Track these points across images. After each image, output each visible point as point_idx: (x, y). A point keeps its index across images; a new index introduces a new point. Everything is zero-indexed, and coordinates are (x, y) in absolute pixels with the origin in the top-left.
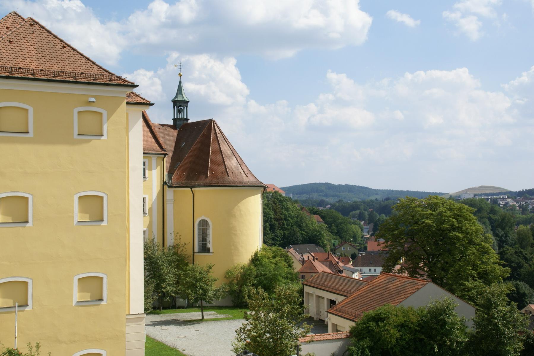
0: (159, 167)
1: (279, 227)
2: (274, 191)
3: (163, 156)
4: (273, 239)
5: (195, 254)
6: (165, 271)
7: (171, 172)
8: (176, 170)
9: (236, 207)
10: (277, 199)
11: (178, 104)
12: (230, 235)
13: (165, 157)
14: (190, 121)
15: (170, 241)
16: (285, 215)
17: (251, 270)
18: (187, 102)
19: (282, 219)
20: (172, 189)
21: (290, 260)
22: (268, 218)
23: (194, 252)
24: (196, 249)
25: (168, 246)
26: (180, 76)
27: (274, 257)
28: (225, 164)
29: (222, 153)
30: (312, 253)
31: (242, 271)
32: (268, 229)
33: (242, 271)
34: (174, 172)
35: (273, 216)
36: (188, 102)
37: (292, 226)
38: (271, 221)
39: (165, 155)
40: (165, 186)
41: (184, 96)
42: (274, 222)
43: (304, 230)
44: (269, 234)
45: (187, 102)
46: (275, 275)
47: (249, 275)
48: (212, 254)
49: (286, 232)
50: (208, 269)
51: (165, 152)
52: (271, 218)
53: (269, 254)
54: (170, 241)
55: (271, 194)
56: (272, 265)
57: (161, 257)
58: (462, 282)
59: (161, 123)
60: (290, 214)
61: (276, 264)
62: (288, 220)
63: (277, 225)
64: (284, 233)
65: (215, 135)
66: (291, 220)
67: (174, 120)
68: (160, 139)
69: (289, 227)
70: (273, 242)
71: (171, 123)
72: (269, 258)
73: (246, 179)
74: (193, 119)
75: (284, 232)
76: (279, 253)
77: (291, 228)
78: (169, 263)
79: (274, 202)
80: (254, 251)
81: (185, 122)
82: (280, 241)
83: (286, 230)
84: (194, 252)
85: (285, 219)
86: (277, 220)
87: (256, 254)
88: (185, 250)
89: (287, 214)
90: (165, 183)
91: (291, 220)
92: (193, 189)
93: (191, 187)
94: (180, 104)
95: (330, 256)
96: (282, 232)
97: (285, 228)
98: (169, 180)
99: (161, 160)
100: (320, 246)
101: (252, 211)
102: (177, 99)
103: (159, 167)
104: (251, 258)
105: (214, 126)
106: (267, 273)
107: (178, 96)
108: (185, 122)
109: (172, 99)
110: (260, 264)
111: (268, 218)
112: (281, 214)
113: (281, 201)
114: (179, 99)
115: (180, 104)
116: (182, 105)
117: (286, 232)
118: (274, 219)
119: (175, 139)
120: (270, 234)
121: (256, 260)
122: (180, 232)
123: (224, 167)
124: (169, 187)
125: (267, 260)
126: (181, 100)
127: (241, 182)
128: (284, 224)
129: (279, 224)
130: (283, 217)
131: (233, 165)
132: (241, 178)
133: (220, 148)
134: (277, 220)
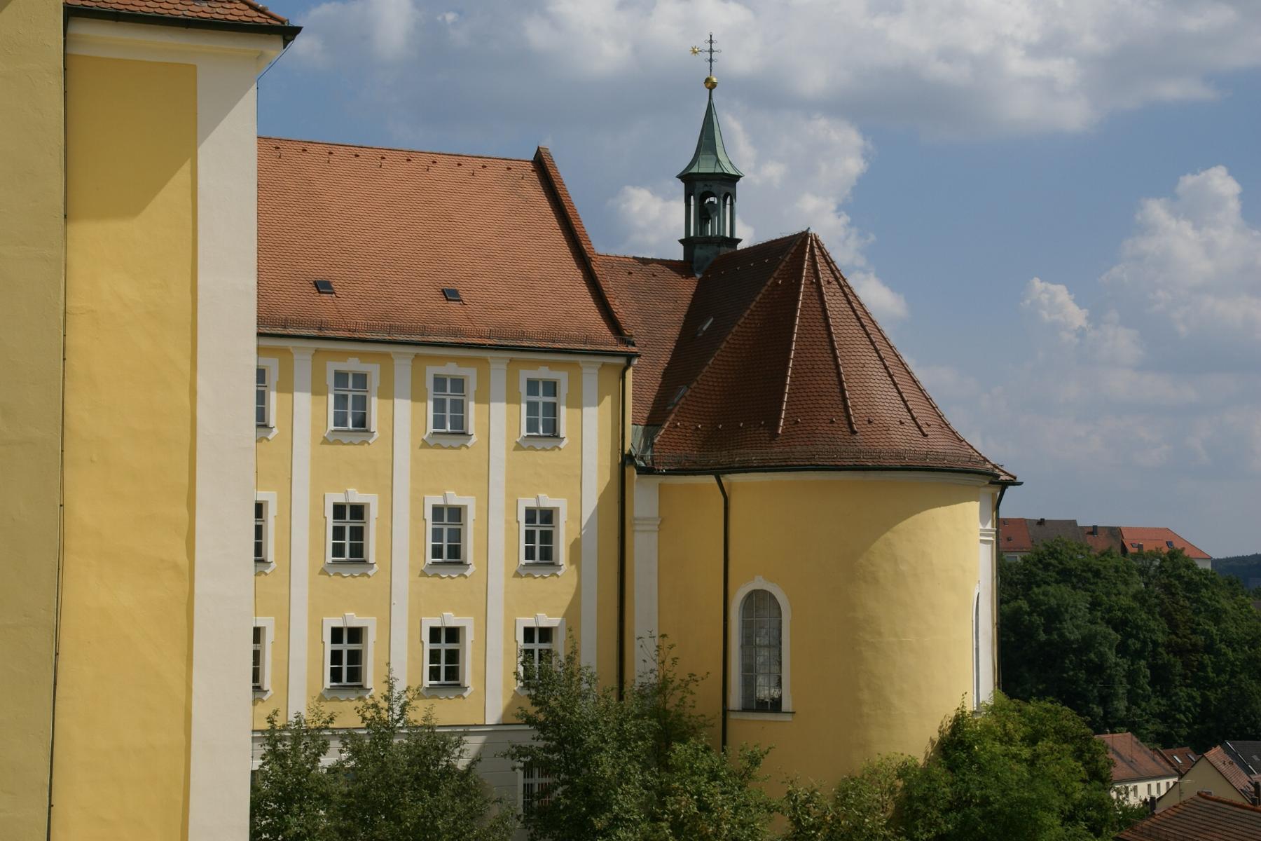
0: (608, 399)
1: (1185, 677)
2: (1166, 550)
3: (622, 361)
4: (1163, 717)
5: (732, 716)
6: (606, 766)
7: (652, 423)
8: (670, 412)
10: (1179, 577)
11: (700, 187)
12: (855, 651)
13: (629, 364)
14: (740, 247)
15: (642, 667)
16: (1206, 633)
17: (931, 780)
18: (735, 178)
19: (1195, 648)
20: (654, 481)
21: (1098, 752)
22: (1144, 643)
23: (725, 711)
24: (735, 700)
25: (638, 681)
26: (710, 85)
27: (1032, 740)
28: (843, 391)
29: (833, 350)
31: (900, 783)
32: (1143, 681)
33: (900, 783)
34: (664, 421)
35: (1161, 638)
36: (737, 178)
37: (1233, 674)
38: (1155, 654)
39: (630, 357)
40: (627, 470)
41: (721, 156)
42: (1165, 657)
44: (1147, 698)
45: (735, 178)
46: (1024, 802)
47: (924, 799)
48: (788, 718)
49: (1211, 695)
50: (746, 764)
51: (634, 349)
52: (1155, 643)
53: (1017, 728)
54: (642, 667)
55: (1157, 563)
56: (1017, 767)
57: (595, 722)
59: (641, 256)
60: (1225, 631)
61: (1032, 763)
62: (1218, 653)
63: (1179, 668)
64: (1206, 700)
65: (813, 289)
66: (1230, 654)
67: (687, 242)
68: (616, 305)
69: (1224, 677)
70: (1162, 728)
71: (678, 254)
72: (1007, 739)
73: (921, 445)
74: (747, 235)
75: (1203, 695)
76: (1050, 726)
77: (1228, 682)
78: (623, 742)
79: (1167, 588)
81: (725, 250)
82: (1189, 725)
83: (1213, 686)
84: (725, 711)
85: (1209, 648)
86: (1178, 651)
87: (959, 722)
88: (689, 700)
89: (1214, 630)
90: (626, 461)
91: (1230, 654)
92: (725, 479)
93: (718, 472)
94: (708, 188)
96: (1196, 694)
97: (1206, 678)
98: (646, 448)
99: (615, 376)
101: (951, 569)
102: (694, 170)
103: (608, 399)
105: (813, 256)
106: (993, 794)
107: (702, 157)
108: (725, 250)
109: (681, 167)
110: (973, 759)
111: (1144, 643)
112: (1194, 632)
113: (1191, 587)
114: (705, 167)
115: (708, 188)
116: (714, 189)
118: (1169, 647)
119: (685, 309)
120: (1153, 701)
121: (956, 743)
122: (676, 634)
123: (838, 399)
124: (643, 471)
125: (998, 748)
126: (711, 171)
127: (898, 455)
128: (1202, 667)
129: (1186, 665)
130: (1200, 640)
131: (873, 395)
132: (903, 439)
133: (830, 334)
134: (1178, 651)
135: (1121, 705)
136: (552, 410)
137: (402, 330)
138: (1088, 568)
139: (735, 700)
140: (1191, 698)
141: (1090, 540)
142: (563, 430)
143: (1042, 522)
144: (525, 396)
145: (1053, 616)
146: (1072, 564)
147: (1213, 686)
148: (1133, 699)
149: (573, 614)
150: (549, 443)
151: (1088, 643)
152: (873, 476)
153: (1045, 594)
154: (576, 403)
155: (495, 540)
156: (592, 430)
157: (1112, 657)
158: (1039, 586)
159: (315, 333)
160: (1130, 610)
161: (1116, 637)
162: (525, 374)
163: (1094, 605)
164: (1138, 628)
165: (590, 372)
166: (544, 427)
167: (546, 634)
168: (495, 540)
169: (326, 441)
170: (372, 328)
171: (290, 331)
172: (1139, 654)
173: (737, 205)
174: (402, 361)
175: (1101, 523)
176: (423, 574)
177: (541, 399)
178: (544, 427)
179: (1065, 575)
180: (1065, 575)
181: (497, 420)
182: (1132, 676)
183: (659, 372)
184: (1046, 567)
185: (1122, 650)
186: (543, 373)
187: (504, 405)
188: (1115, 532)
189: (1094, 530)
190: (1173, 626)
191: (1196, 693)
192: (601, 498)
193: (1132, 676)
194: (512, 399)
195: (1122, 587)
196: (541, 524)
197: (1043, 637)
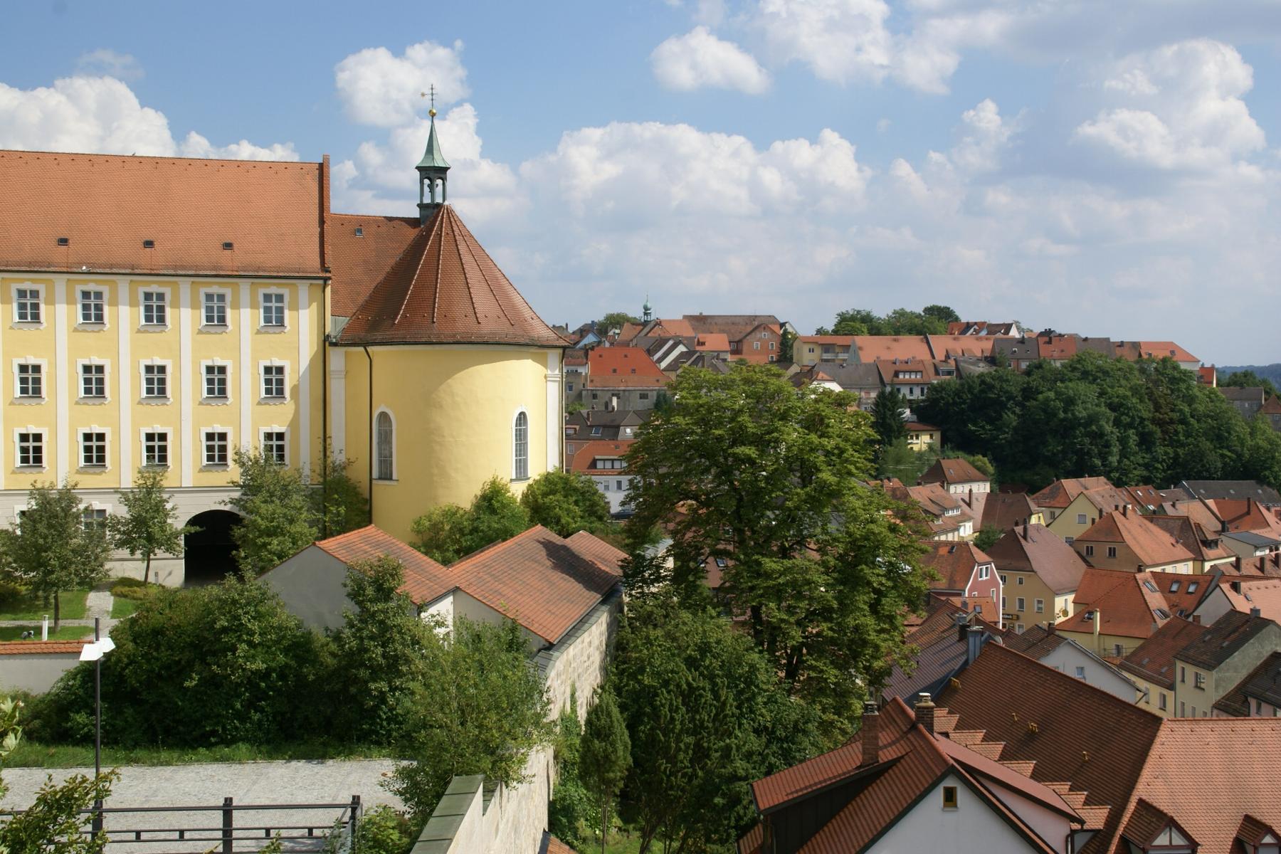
0: (314, 305)
3: (321, 282)
9: (443, 386)
16: (1181, 411)
19: (1172, 422)
24: (375, 474)
30: (1210, 502)
35: (1145, 414)
39: (326, 279)
43: (1228, 448)
49: (1180, 451)
51: (328, 275)
52: (1142, 420)
58: (756, 557)
63: (1159, 434)
64: (1177, 454)
66: (1196, 426)
67: (422, 206)
69: (1190, 440)
70: (1145, 473)
71: (415, 213)
80: (489, 478)
82: (1164, 471)
83: (1183, 445)
85: (1183, 421)
86: (1159, 423)
89: (1187, 409)
91: (1196, 426)
92: (369, 349)
93: (365, 345)
95: (1253, 508)
97: (1179, 441)
100: (1269, 485)
104: (479, 493)
111: (1133, 418)
112: (1172, 411)
117: (1180, 451)
118: (1154, 421)
128: (1176, 433)
130: (1175, 416)
132: (491, 324)
135: (1114, 460)
136: (280, 310)
137: (184, 267)
138: (1100, 369)
140: (1166, 453)
141: (1119, 351)
142: (286, 322)
143: (1086, 339)
144: (262, 304)
145: (1070, 402)
146: (1090, 368)
147: (1183, 445)
148: (1124, 454)
149: (294, 424)
150: (278, 330)
151: (1092, 419)
152: (437, 347)
153: (1066, 388)
154: (295, 307)
155: (246, 384)
156: (306, 321)
157: (1108, 428)
158: (1062, 381)
159: (128, 271)
160: (1125, 397)
161: (1112, 415)
162: (262, 291)
163: (1102, 394)
164: (1129, 409)
165: (303, 288)
166: (275, 319)
167: (280, 436)
168: (246, 384)
169: (139, 331)
170: (167, 267)
171: (114, 270)
172: (1130, 425)
173: (448, 184)
174: (185, 286)
175: (1125, 340)
176: (201, 404)
177: (274, 304)
178: (275, 319)
179: (1085, 375)
180: (1085, 375)
181: (245, 318)
182: (1123, 441)
183: (373, 286)
184: (1074, 369)
185: (1117, 423)
186: (273, 290)
187: (249, 310)
188: (1136, 346)
189: (1122, 344)
190: (1157, 408)
191: (1170, 450)
192: (311, 361)
193: (1123, 441)
194: (254, 306)
195: (1123, 382)
196: (274, 376)
197: (1062, 415)
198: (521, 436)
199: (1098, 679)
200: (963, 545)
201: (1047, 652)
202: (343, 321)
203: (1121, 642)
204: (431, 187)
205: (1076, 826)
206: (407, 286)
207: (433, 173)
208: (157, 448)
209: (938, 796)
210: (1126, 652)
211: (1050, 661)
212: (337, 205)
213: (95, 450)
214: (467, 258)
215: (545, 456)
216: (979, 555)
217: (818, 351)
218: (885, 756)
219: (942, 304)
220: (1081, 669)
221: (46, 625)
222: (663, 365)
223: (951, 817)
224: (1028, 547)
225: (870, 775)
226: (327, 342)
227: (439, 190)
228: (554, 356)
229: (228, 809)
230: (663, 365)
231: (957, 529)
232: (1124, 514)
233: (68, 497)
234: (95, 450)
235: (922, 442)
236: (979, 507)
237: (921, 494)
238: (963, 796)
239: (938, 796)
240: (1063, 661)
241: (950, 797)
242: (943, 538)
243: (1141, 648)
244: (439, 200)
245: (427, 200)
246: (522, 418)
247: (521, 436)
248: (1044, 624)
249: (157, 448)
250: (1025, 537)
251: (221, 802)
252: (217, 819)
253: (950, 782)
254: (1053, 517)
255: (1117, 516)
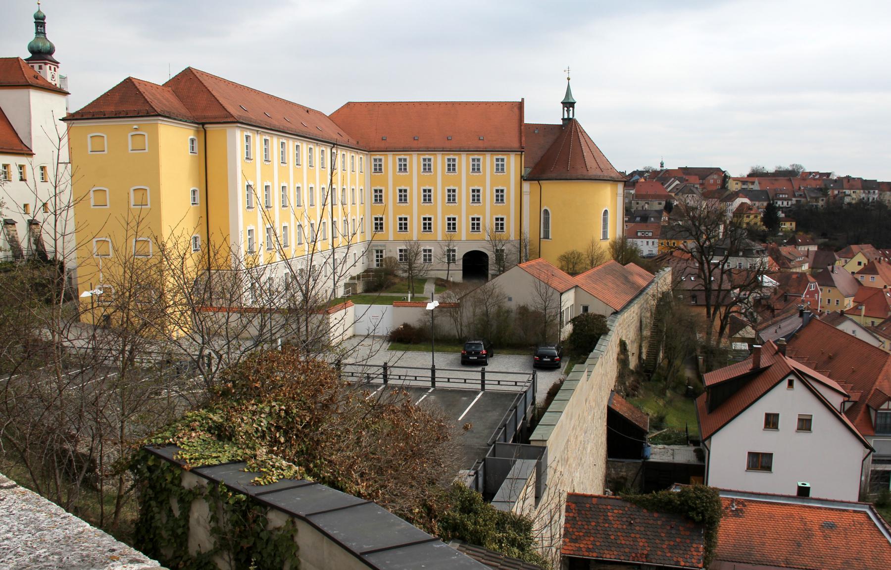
24: (542, 236)
93: (538, 180)
132: (594, 172)
139: (542, 236)
166: (500, 168)
198: (605, 220)
199: (862, 335)
200: (803, 275)
201: (840, 323)
202: (529, 170)
203: (873, 320)
204: (568, 111)
205: (846, 399)
206: (557, 153)
207: (568, 104)
208: (452, 225)
209: (785, 383)
210: (876, 324)
211: (841, 327)
212: (527, 120)
213: (427, 225)
214: (582, 140)
215: (616, 229)
216: (811, 279)
217: (740, 184)
218: (762, 366)
219: (786, 165)
220: (854, 332)
221: (410, 295)
222: (669, 189)
223: (790, 392)
224: (834, 276)
225: (757, 372)
226: (523, 179)
227: (571, 112)
228: (620, 188)
229: (385, 367)
230: (669, 189)
231: (801, 266)
232: (879, 262)
233: (418, 244)
234: (427, 225)
235: (788, 226)
236: (811, 257)
237: (785, 250)
238: (796, 383)
239: (785, 383)
240: (847, 327)
241: (791, 383)
242: (794, 270)
243: (883, 323)
244: (571, 116)
245: (566, 117)
246: (606, 212)
247: (605, 220)
248: (839, 311)
249: (452, 225)
250: (832, 271)
251: (382, 364)
252: (429, 374)
253: (791, 377)
254: (846, 262)
255: (876, 262)
